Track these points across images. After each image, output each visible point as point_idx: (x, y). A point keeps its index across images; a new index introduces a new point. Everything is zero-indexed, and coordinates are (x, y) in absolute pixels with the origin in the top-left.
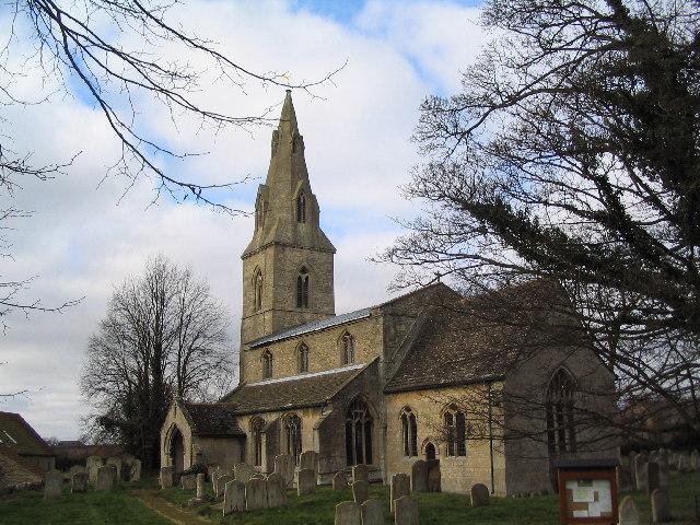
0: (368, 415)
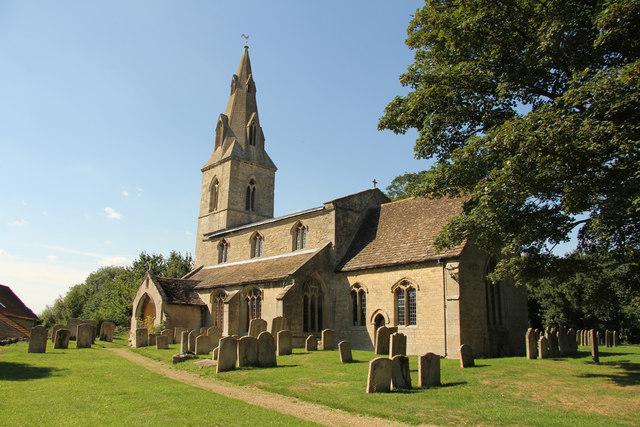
0: (320, 291)
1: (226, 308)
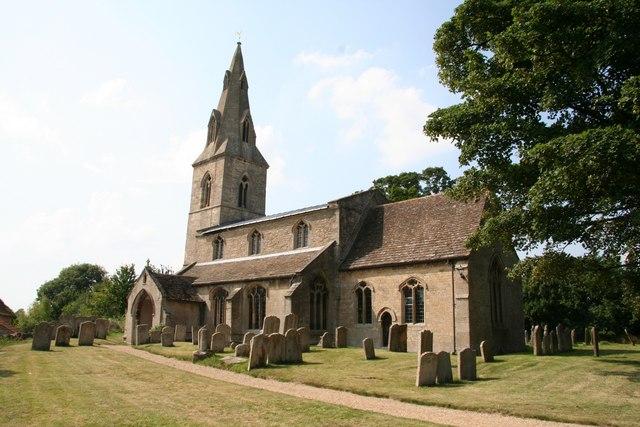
0: (325, 289)
1: (229, 306)
